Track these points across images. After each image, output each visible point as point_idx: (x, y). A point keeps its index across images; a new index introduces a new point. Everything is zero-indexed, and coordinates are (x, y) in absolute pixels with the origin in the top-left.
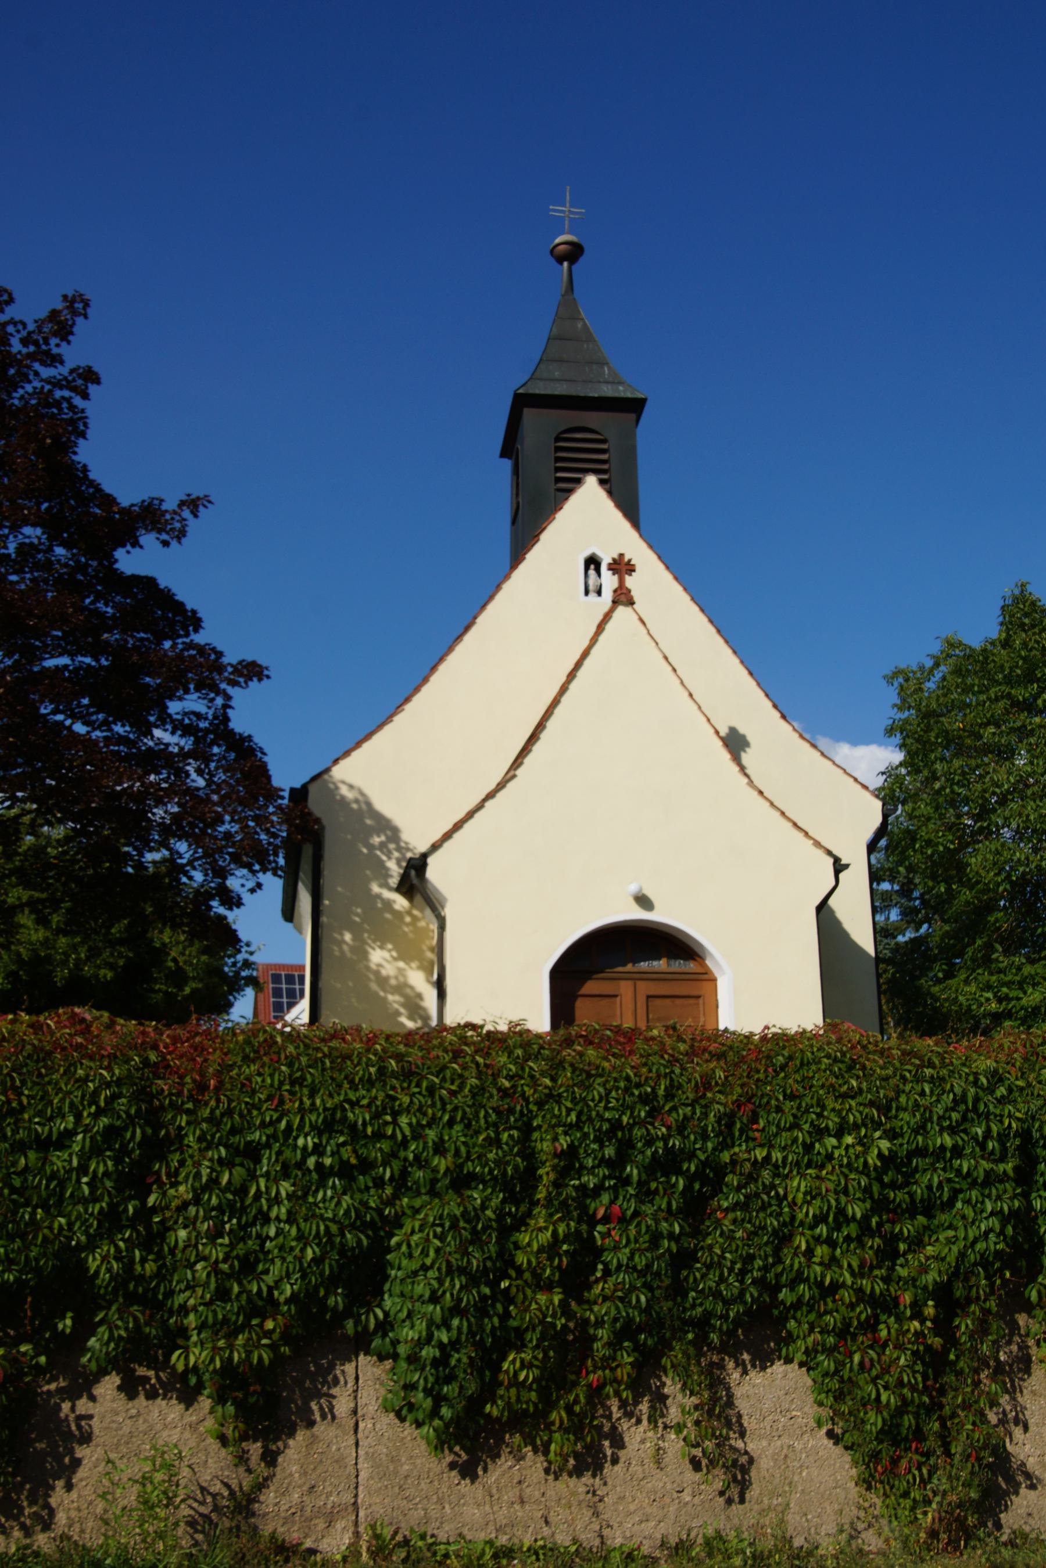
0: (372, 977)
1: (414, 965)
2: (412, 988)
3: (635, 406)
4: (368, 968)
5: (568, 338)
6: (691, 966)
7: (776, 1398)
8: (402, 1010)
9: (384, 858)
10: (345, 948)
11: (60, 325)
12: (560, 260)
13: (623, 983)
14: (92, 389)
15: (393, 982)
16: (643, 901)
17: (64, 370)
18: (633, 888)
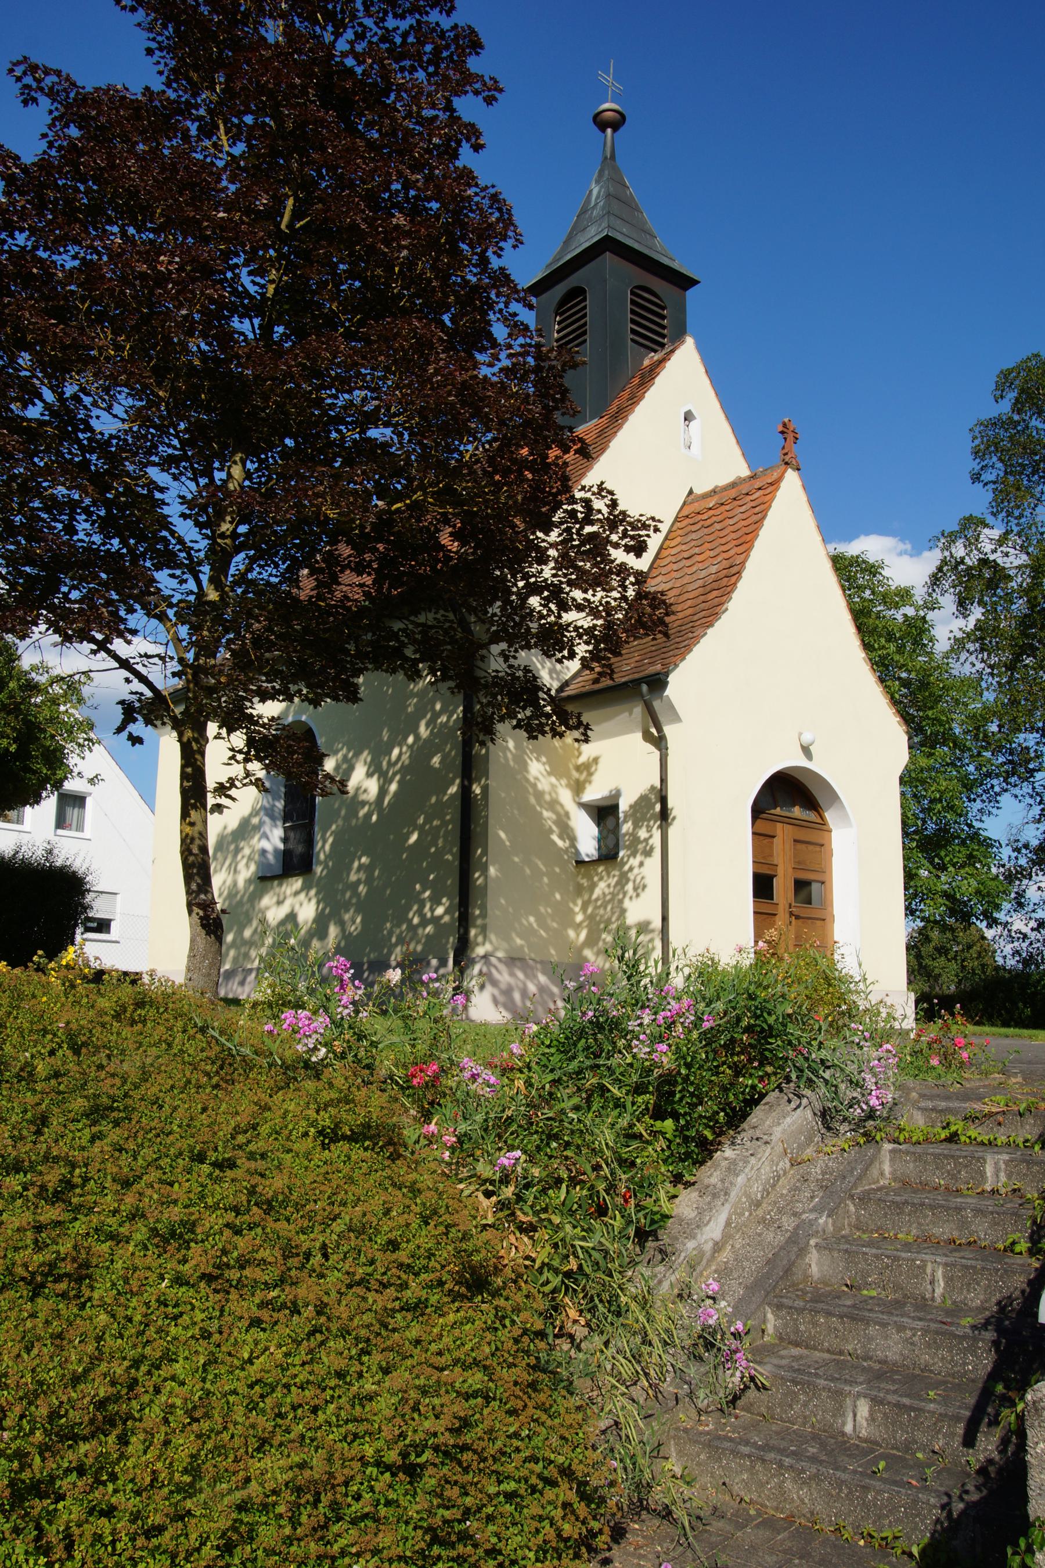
0: (531, 790)
1: (564, 782)
2: (562, 806)
4: (527, 780)
5: (619, 200)
6: (812, 816)
8: (554, 828)
9: (539, 666)
10: (509, 755)
13: (779, 825)
15: (547, 797)
16: (806, 751)
18: (807, 738)
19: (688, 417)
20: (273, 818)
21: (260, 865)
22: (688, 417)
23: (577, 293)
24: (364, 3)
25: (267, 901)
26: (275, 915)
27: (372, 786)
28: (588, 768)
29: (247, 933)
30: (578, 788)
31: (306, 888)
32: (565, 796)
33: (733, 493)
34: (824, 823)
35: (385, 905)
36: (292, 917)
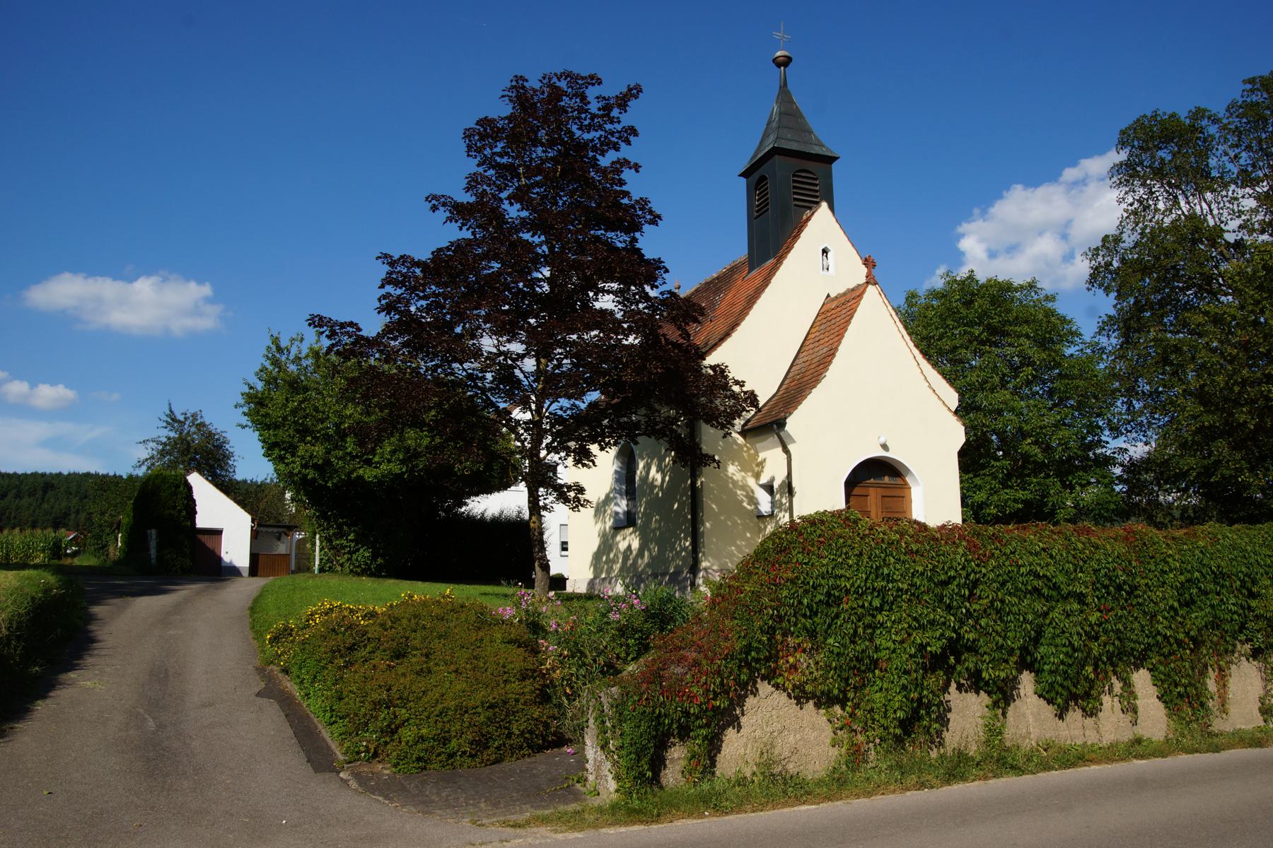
3: (831, 160)
5: (789, 114)
6: (899, 481)
7: (1142, 679)
11: (623, 101)
12: (779, 65)
14: (632, 138)
16: (885, 447)
17: (619, 127)
18: (882, 440)
19: (825, 251)
20: (621, 495)
21: (616, 521)
22: (825, 251)
23: (763, 178)
24: (6, 565)
25: (619, 538)
26: (623, 546)
27: (659, 477)
28: (761, 464)
29: (612, 556)
30: (757, 476)
31: (634, 532)
32: (751, 482)
33: (843, 300)
34: (906, 484)
35: (665, 542)
36: (629, 547)
